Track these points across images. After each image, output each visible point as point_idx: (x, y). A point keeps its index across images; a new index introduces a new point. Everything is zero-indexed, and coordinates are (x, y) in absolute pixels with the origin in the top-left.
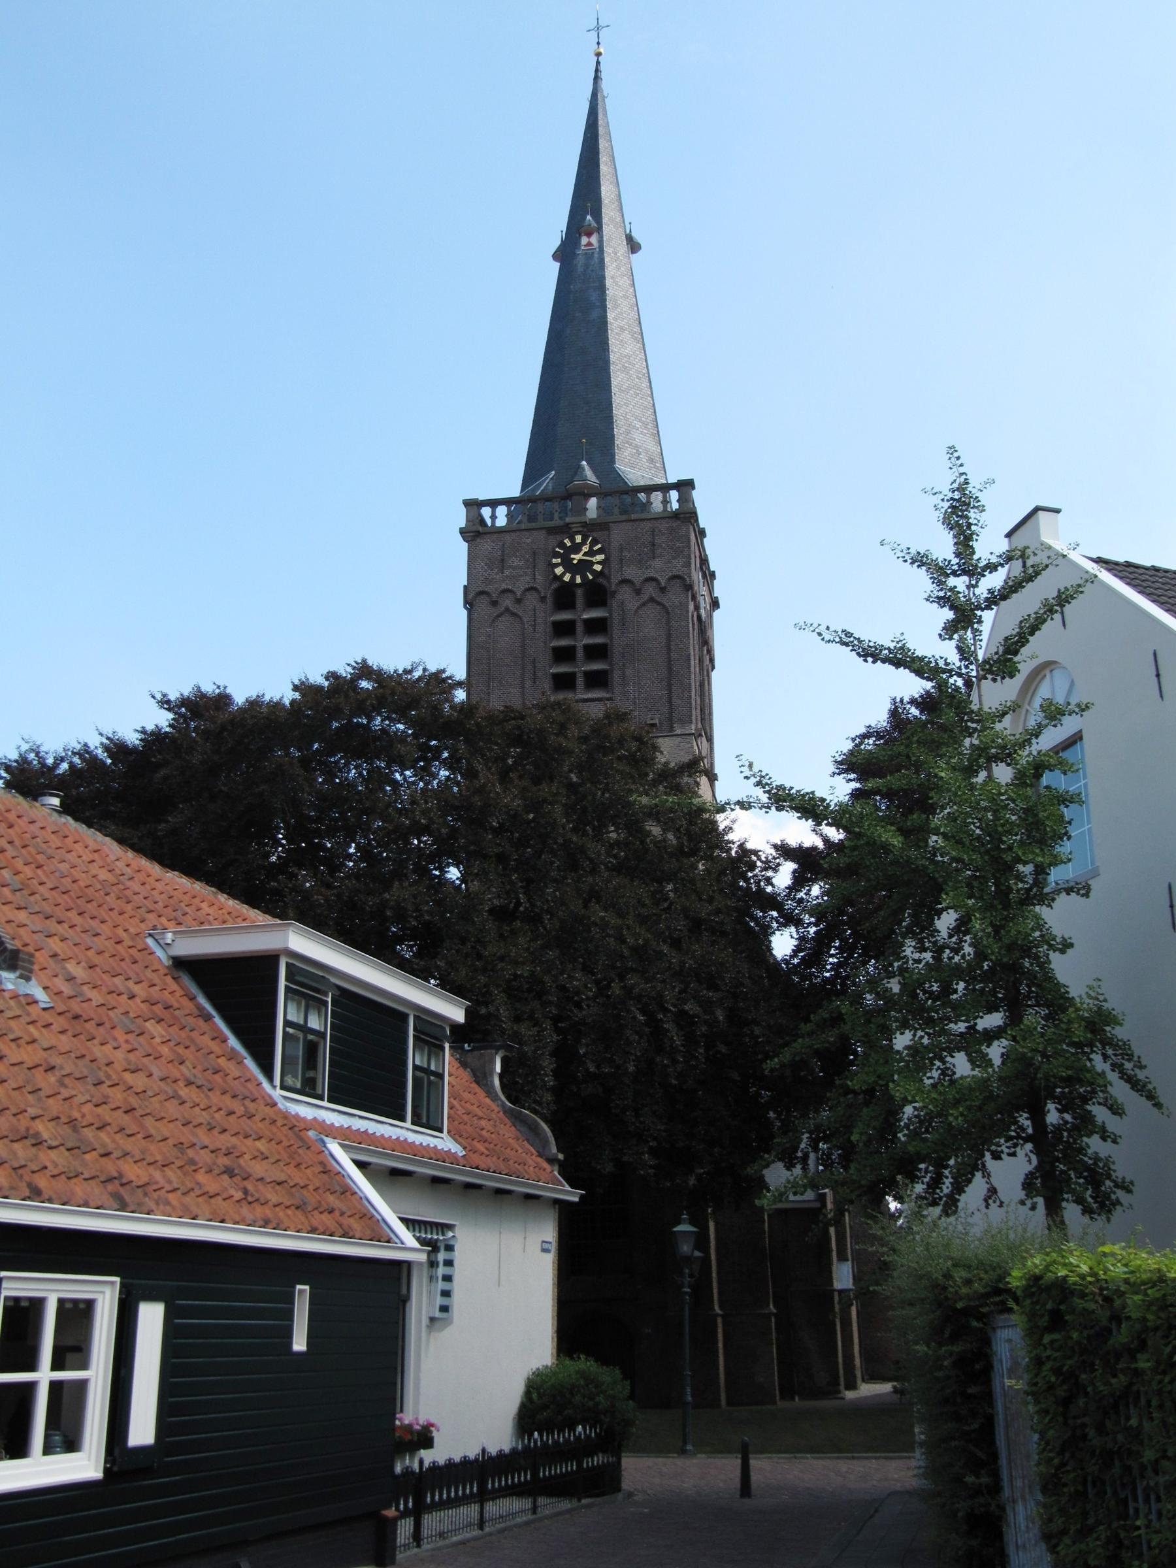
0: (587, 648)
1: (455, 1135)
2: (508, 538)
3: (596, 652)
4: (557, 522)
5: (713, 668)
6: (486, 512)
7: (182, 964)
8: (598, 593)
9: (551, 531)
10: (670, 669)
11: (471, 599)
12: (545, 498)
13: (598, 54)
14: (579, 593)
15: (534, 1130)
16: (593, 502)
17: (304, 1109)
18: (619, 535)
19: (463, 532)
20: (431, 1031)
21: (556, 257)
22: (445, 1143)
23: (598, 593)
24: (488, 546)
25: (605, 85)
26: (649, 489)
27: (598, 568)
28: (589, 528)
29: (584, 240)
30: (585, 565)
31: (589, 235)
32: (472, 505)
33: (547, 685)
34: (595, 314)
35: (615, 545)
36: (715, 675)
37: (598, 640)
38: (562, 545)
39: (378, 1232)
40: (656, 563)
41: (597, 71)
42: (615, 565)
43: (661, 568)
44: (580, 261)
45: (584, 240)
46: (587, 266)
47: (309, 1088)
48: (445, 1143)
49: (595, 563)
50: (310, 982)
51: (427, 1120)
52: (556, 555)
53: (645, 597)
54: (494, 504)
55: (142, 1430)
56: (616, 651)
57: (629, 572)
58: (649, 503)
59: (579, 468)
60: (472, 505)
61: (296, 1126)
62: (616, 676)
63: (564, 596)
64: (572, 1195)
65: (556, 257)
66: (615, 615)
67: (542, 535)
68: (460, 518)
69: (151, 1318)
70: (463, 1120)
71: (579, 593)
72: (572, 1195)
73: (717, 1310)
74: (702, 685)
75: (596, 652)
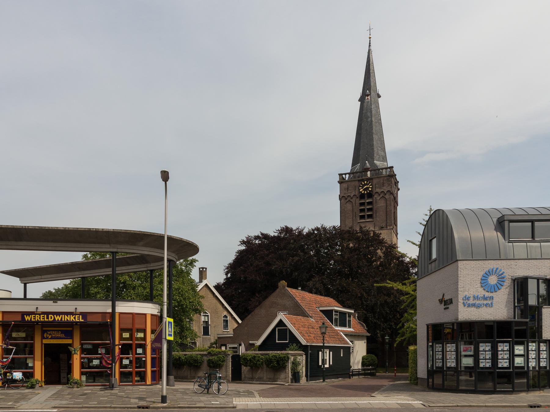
0: (367, 209)
1: (353, 328)
2: (349, 183)
3: (369, 210)
4: (360, 178)
5: (397, 205)
6: (344, 176)
7: (321, 311)
8: (370, 195)
9: (359, 181)
10: (387, 214)
11: (341, 198)
12: (356, 173)
13: (370, 38)
14: (366, 195)
15: (362, 325)
16: (369, 173)
17: (337, 328)
18: (375, 181)
19: (338, 182)
20: (350, 314)
21: (359, 101)
22: (352, 330)
23: (370, 195)
24: (345, 185)
25: (372, 48)
26: (382, 169)
27: (370, 189)
28: (368, 180)
29: (367, 98)
30: (367, 188)
31: (368, 96)
32: (341, 175)
33: (358, 218)
34: (369, 119)
35: (374, 183)
36: (398, 208)
37: (370, 207)
38: (362, 184)
39: (348, 344)
40: (385, 188)
41: (370, 43)
42: (374, 189)
43: (386, 189)
44: (365, 104)
45: (367, 98)
46: (367, 105)
47: (336, 325)
48: (352, 330)
49: (369, 186)
50: (336, 311)
51: (350, 327)
52: (360, 186)
53: (381, 196)
54: (345, 174)
55: (331, 364)
56: (374, 209)
57: (378, 190)
58: (382, 172)
59: (366, 163)
60: (341, 175)
61: (336, 330)
62: (374, 215)
63: (362, 196)
64: (368, 334)
65: (359, 101)
66: (374, 201)
67: (357, 182)
68: (338, 178)
69: (331, 353)
70: (355, 326)
71: (366, 195)
72: (368, 334)
73: (123, 307)
74: (394, 212)
75: (369, 210)
